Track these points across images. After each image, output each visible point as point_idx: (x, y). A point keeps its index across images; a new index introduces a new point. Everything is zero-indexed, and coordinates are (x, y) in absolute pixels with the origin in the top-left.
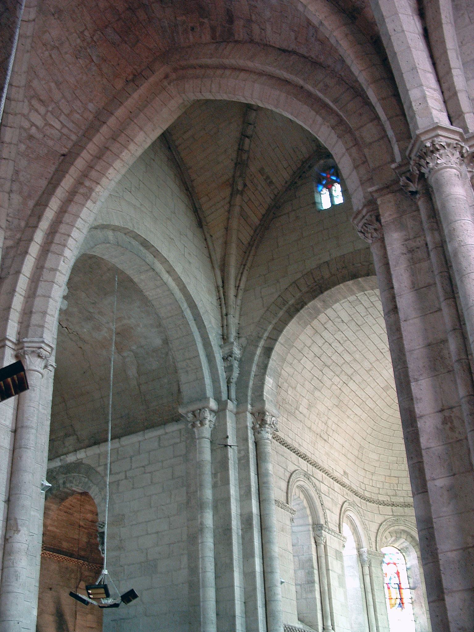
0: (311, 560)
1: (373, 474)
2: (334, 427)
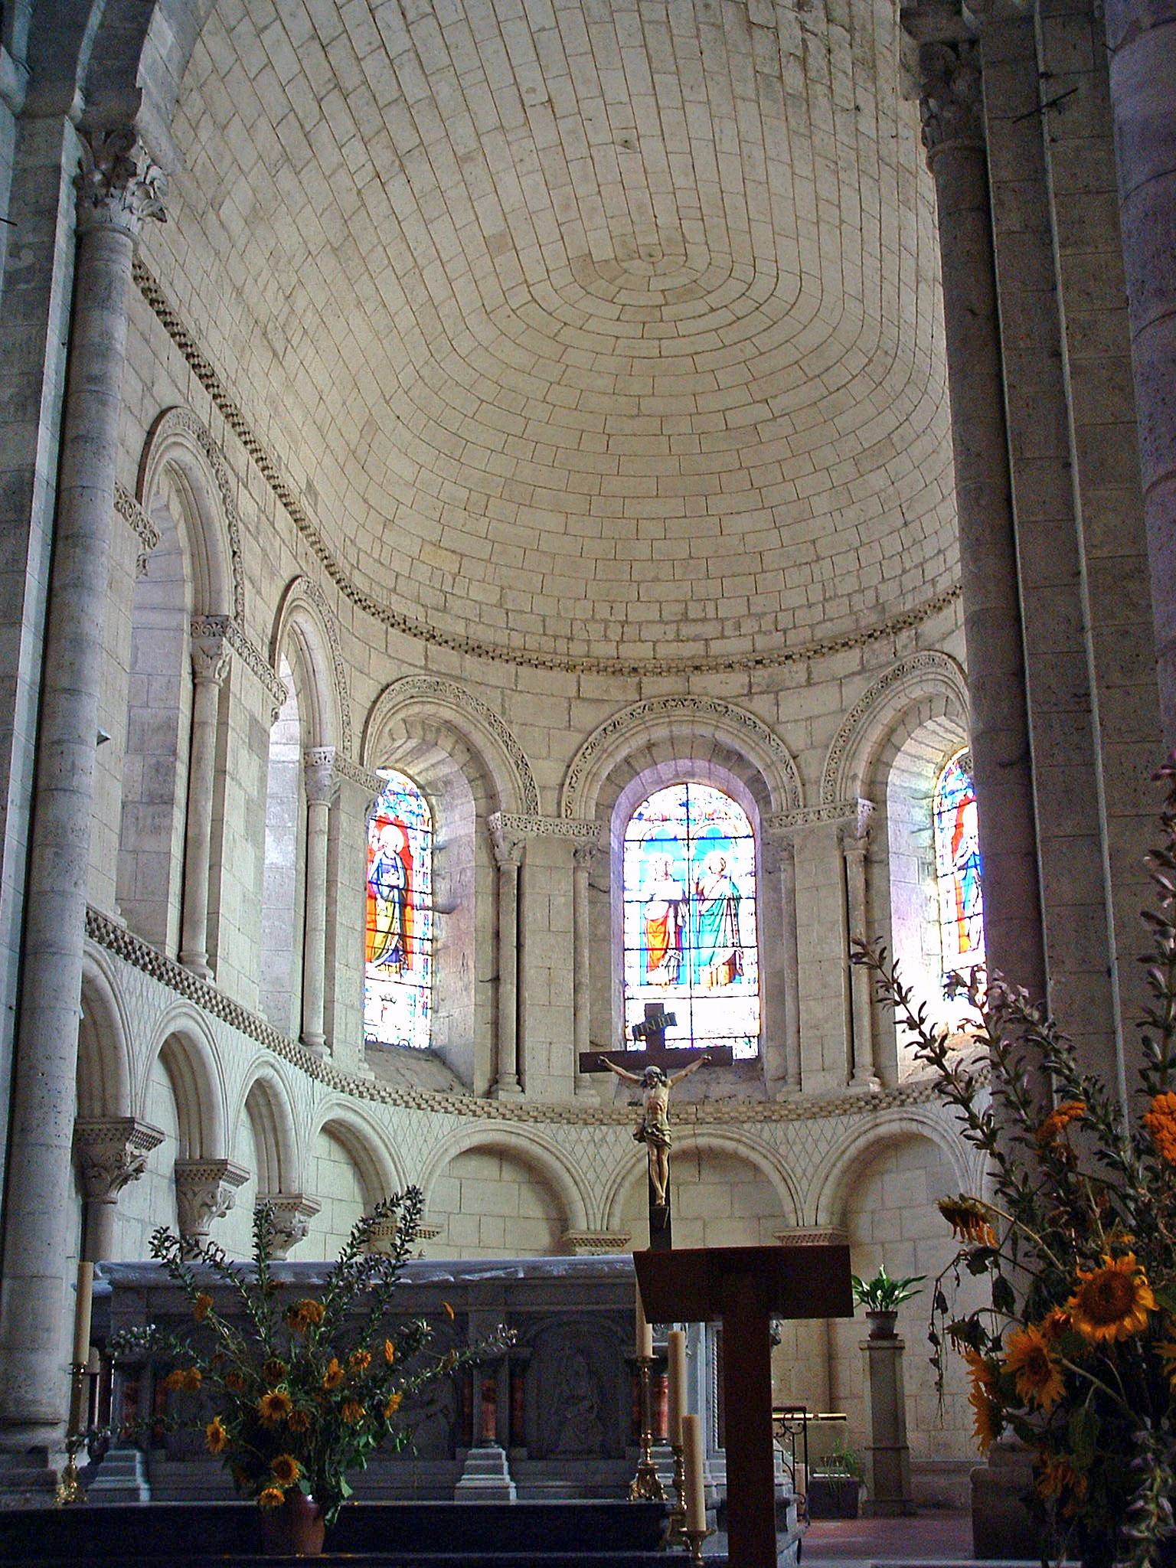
0: (171, 727)
1: (387, 523)
2: (311, 319)
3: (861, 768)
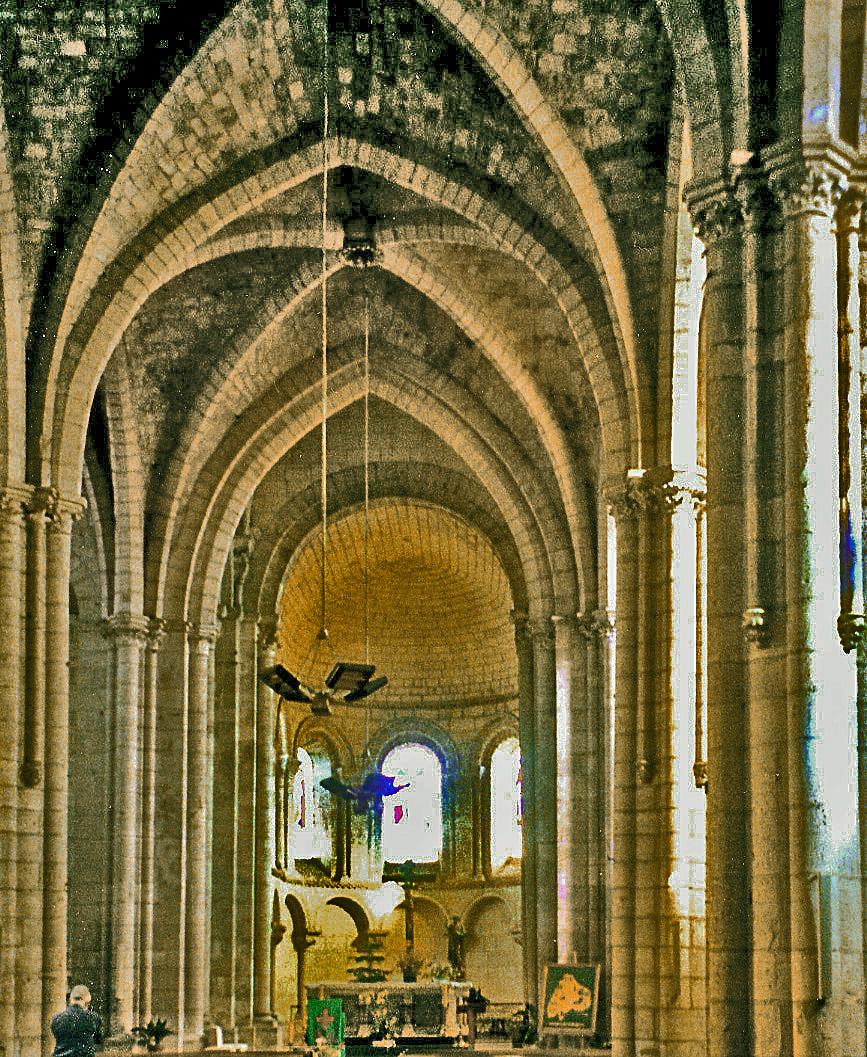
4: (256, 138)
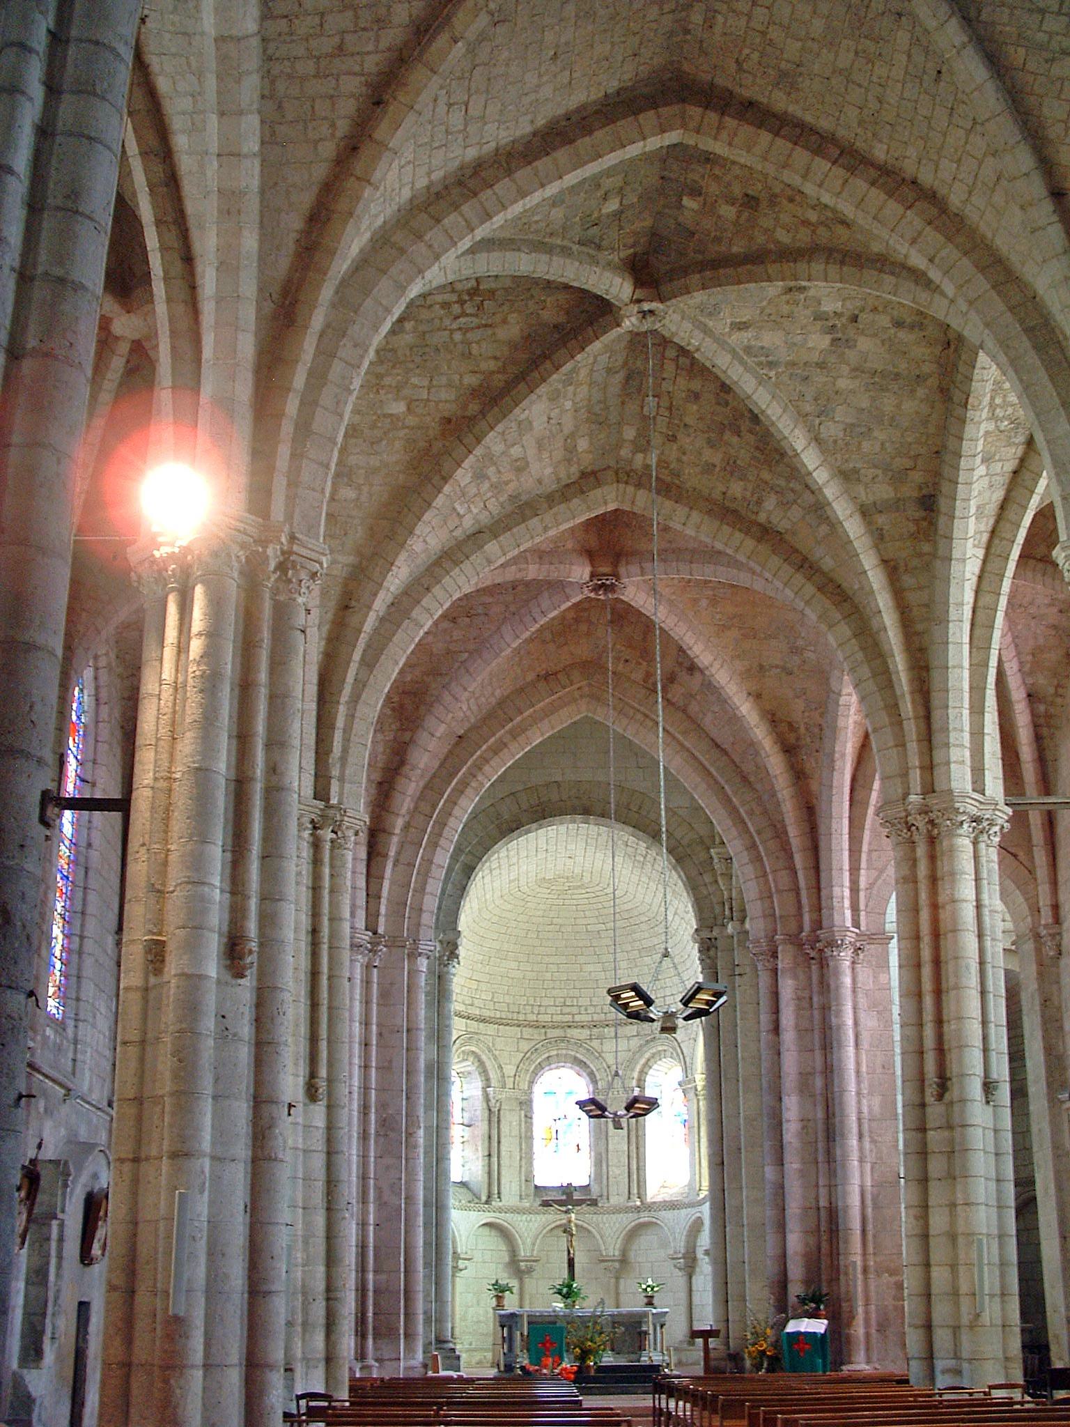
3: (636, 1075)
4: (540, 483)
